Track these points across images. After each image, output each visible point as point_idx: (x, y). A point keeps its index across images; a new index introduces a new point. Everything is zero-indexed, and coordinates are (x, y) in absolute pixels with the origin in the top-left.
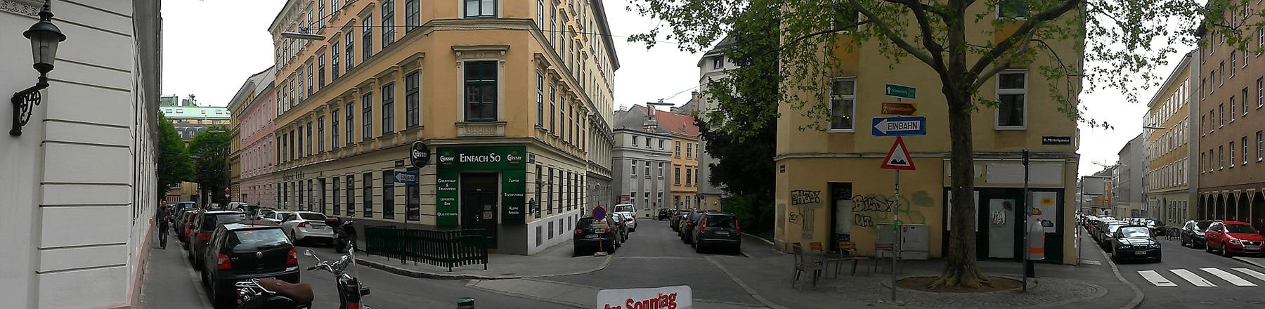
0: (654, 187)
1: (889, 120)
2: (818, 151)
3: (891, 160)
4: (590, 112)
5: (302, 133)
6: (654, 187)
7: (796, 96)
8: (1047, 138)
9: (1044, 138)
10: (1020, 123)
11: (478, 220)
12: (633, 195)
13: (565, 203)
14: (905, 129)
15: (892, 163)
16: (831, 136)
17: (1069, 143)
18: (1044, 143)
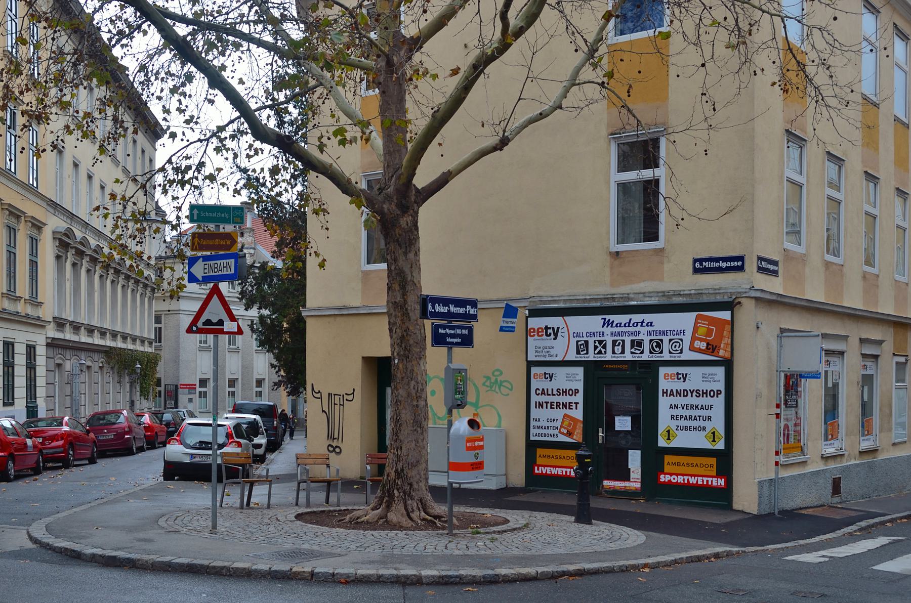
0: (247, 368)
1: (206, 258)
2: (347, 304)
3: (203, 319)
4: (55, 223)
5: (42, 200)
6: (247, 368)
7: (848, 103)
8: (701, 261)
9: (695, 261)
10: (656, 238)
11: (586, 460)
12: (203, 382)
13: (679, 412)
14: (220, 273)
15: (204, 324)
16: (366, 274)
17: (741, 268)
18: (696, 271)
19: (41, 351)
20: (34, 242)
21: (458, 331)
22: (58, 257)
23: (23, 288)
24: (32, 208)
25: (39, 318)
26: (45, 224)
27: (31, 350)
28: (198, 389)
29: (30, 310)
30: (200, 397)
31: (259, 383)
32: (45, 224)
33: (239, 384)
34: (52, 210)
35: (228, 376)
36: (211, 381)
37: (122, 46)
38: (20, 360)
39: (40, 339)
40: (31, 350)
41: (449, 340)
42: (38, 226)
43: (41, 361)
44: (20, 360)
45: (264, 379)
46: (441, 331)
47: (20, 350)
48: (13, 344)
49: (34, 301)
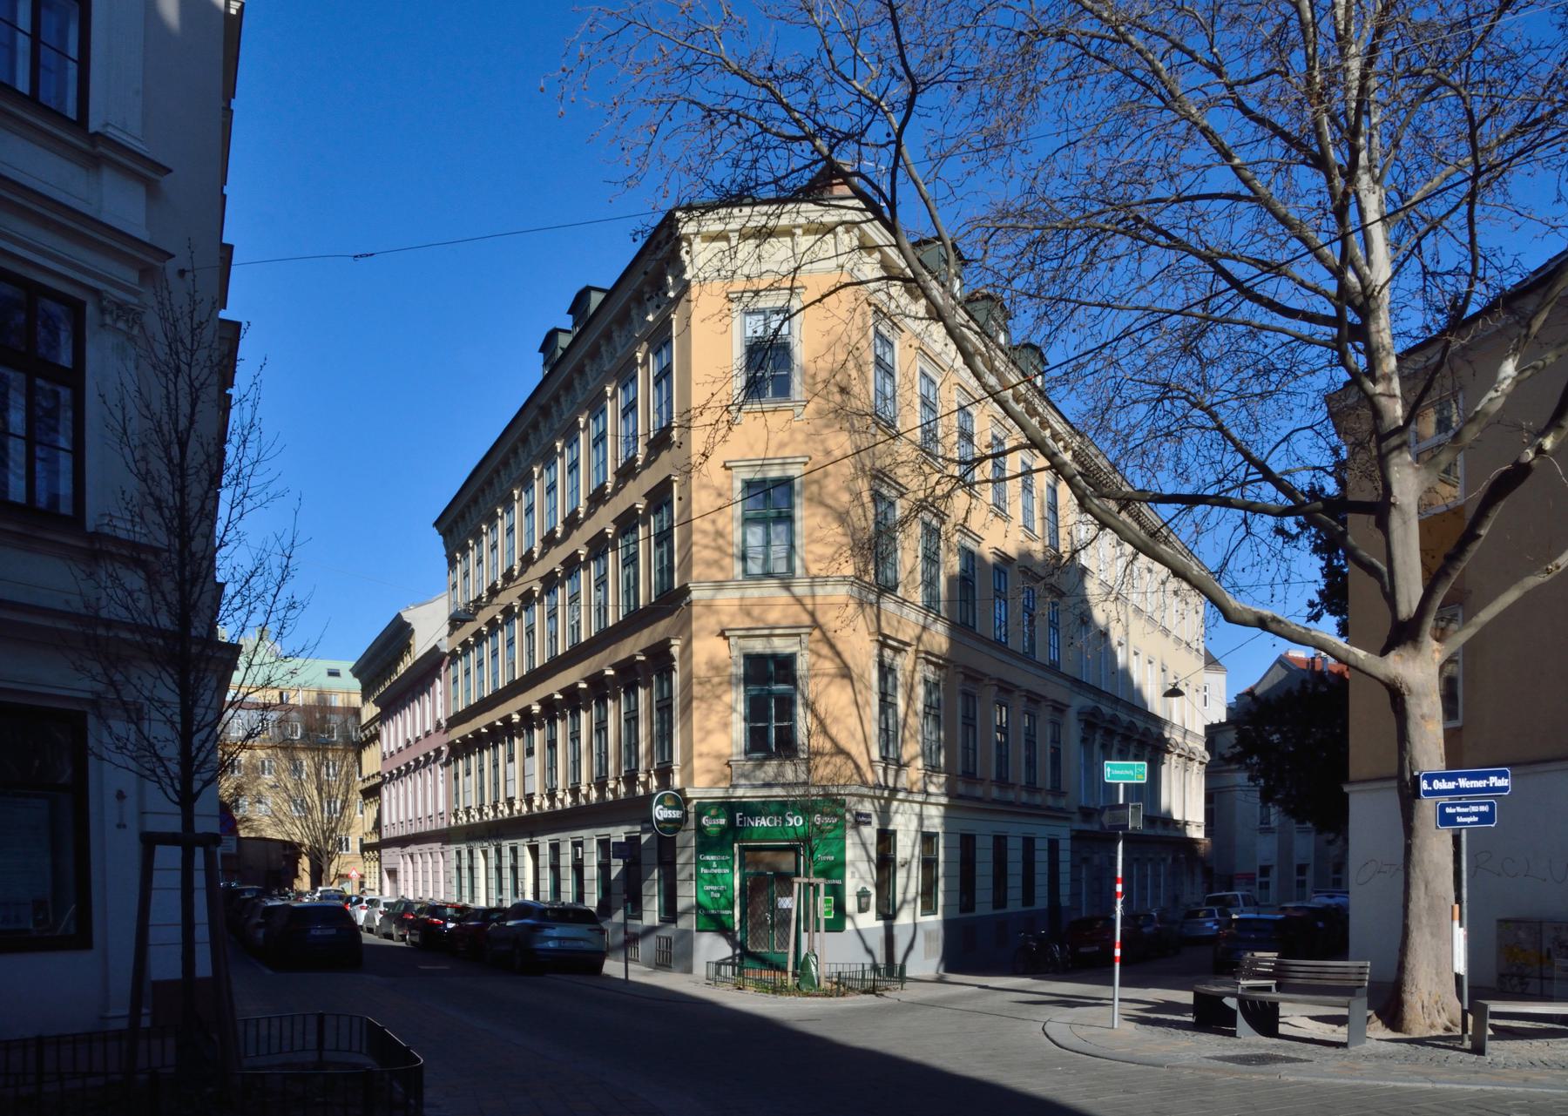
4: (1079, 702)
12: (1265, 871)
19: (1065, 845)
20: (1056, 725)
21: (1474, 809)
22: (1084, 740)
23: (1044, 778)
24: (1055, 690)
25: (1061, 810)
26: (1068, 706)
27: (1053, 845)
28: (1258, 879)
29: (1050, 801)
30: (1261, 888)
31: (1302, 869)
32: (1068, 706)
33: (1274, 874)
34: (1076, 690)
35: (1297, 861)
36: (1276, 868)
37: (1280, 531)
38: (1041, 856)
39: (1063, 832)
40: (1053, 845)
41: (1460, 819)
42: (1059, 708)
43: (1065, 856)
44: (1041, 856)
45: (1271, 866)
46: (1449, 810)
47: (1041, 846)
48: (1005, 838)
49: (1057, 791)
